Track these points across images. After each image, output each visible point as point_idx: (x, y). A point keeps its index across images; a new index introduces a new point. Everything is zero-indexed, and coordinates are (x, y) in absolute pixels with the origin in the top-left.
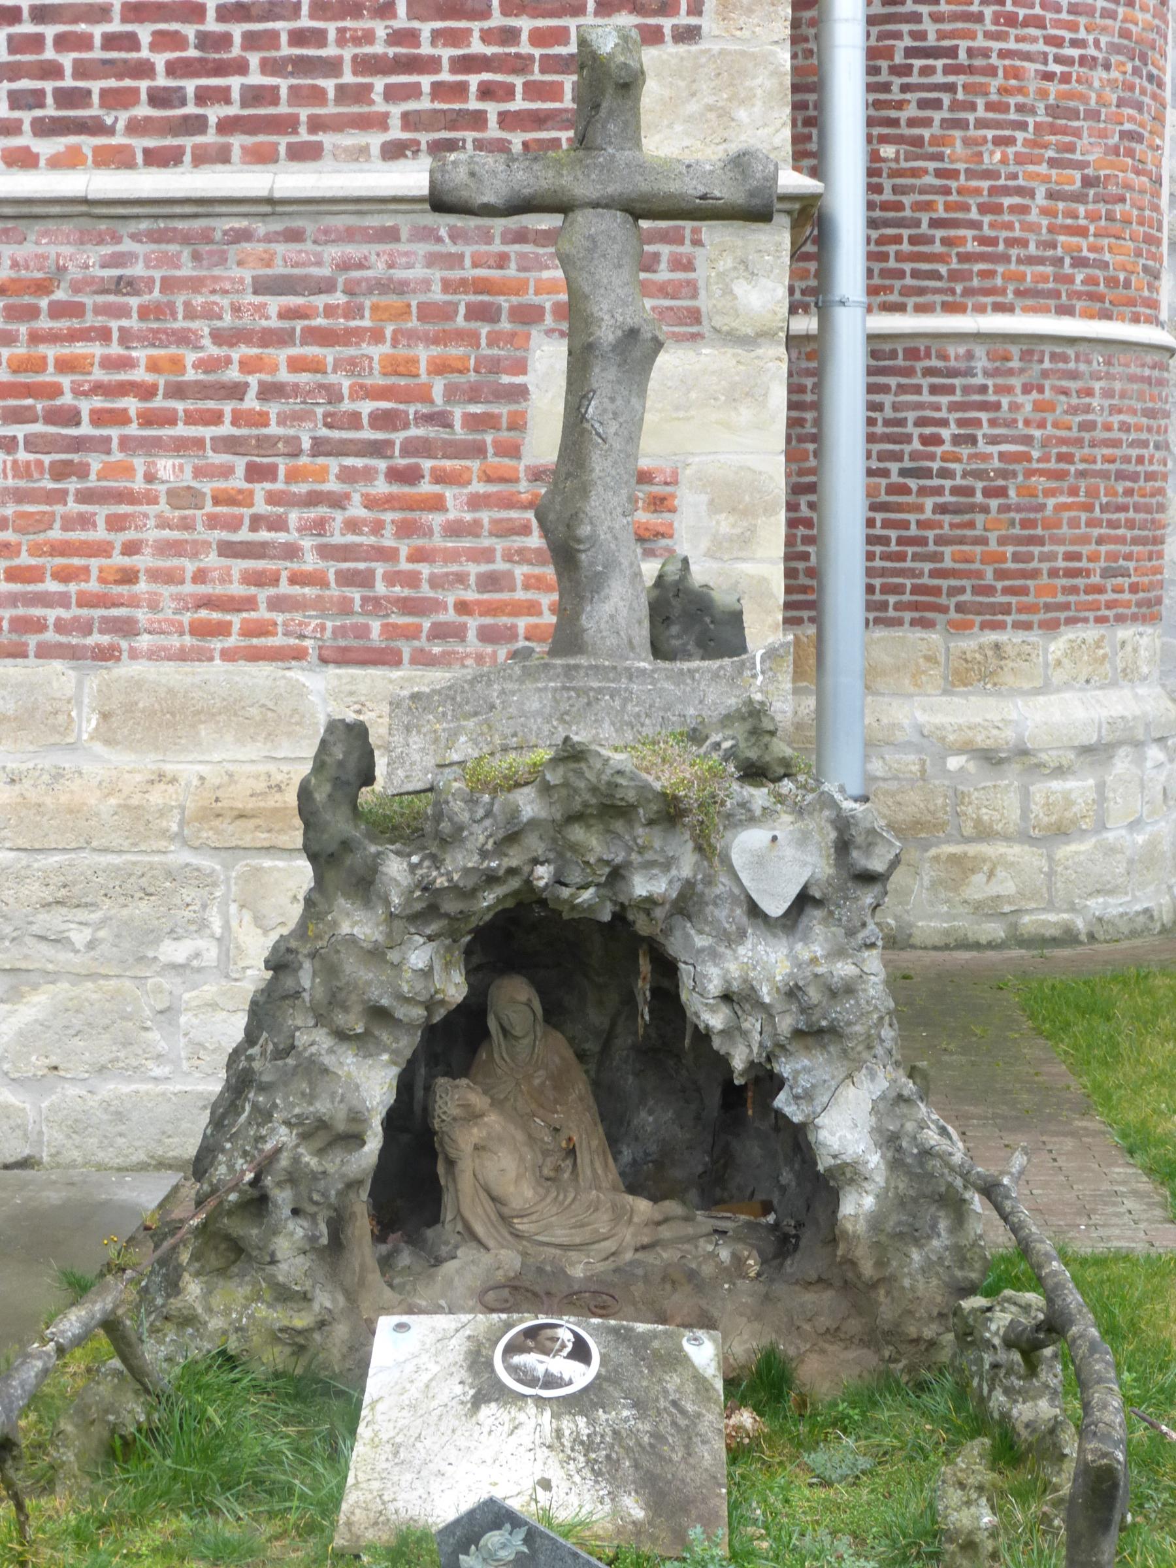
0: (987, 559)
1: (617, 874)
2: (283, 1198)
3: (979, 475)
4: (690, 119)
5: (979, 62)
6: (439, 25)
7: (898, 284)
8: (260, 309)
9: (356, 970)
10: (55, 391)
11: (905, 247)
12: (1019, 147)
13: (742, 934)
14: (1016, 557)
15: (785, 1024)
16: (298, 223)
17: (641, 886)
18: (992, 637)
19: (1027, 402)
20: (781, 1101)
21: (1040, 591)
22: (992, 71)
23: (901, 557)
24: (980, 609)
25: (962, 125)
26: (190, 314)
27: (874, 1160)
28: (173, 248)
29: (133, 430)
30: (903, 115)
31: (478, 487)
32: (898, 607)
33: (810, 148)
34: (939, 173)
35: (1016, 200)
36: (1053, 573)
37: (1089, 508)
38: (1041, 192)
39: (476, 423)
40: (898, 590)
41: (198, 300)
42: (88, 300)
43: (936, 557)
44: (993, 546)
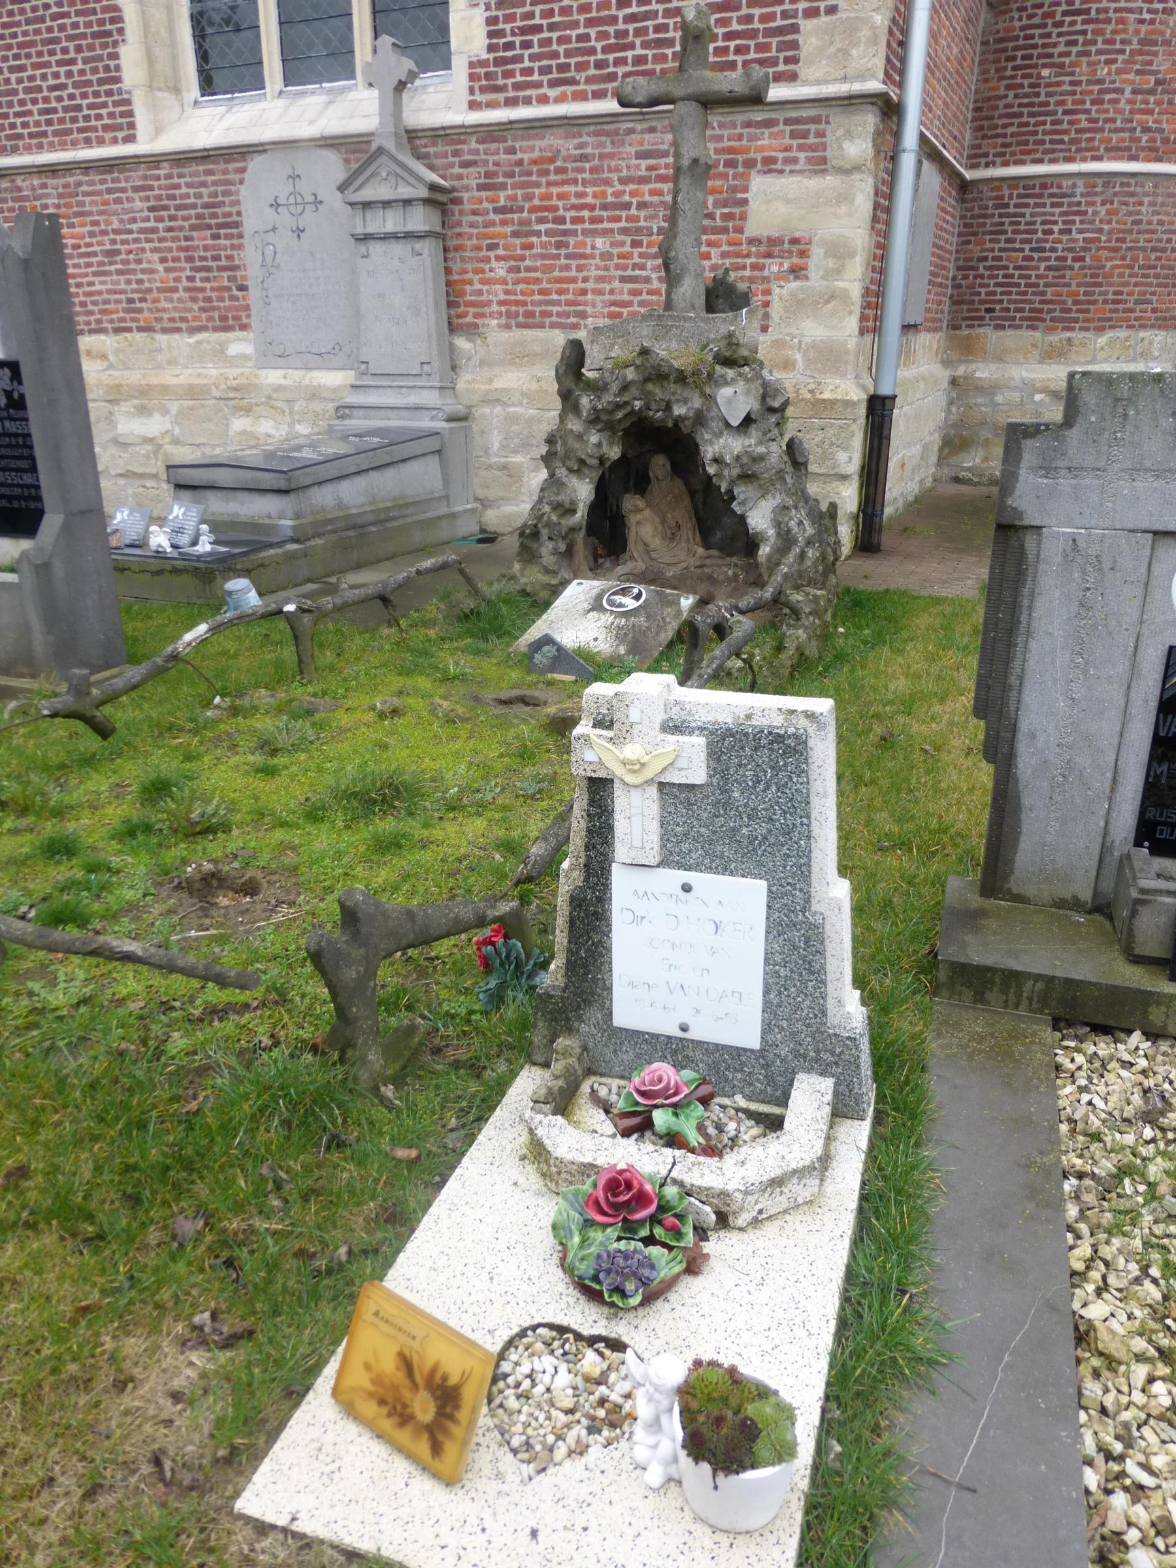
0: (1069, 294)
1: (668, 407)
2: (545, 532)
3: (1071, 250)
4: (829, 57)
5: (1102, 16)
6: (718, 16)
7: (1041, 148)
8: (638, 167)
9: (573, 443)
10: (556, 208)
11: (1048, 127)
12: (1119, 65)
13: (721, 433)
14: (1085, 293)
15: (736, 472)
16: (653, 124)
17: (678, 410)
18: (1068, 334)
19: (1103, 210)
20: (734, 505)
21: (1096, 311)
22: (1109, 21)
23: (1025, 293)
24: (1063, 320)
25: (1087, 54)
26: (610, 171)
27: (771, 532)
28: (603, 139)
29: (587, 226)
30: (1056, 51)
31: (725, 248)
32: (1021, 319)
33: (896, 69)
34: (1072, 83)
35: (1114, 96)
36: (1105, 302)
37: (1131, 267)
38: (1128, 90)
39: (727, 217)
40: (1022, 310)
41: (613, 163)
42: (569, 165)
43: (1044, 293)
44: (1074, 287)
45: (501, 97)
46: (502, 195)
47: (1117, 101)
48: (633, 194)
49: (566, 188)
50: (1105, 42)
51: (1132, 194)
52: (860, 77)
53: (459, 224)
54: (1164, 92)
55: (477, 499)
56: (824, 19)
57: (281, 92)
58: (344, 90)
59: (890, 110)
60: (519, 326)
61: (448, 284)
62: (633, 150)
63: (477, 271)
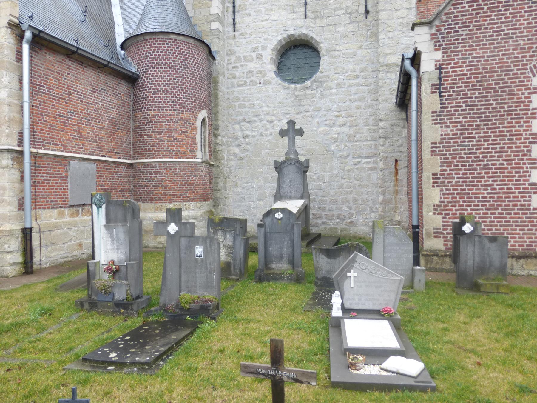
3: (158, 181)
18: (161, 204)
19: (165, 171)
25: (154, 132)
33: (21, 142)
36: (170, 195)
38: (166, 141)
43: (152, 193)
47: (163, 144)
52: (4, 145)
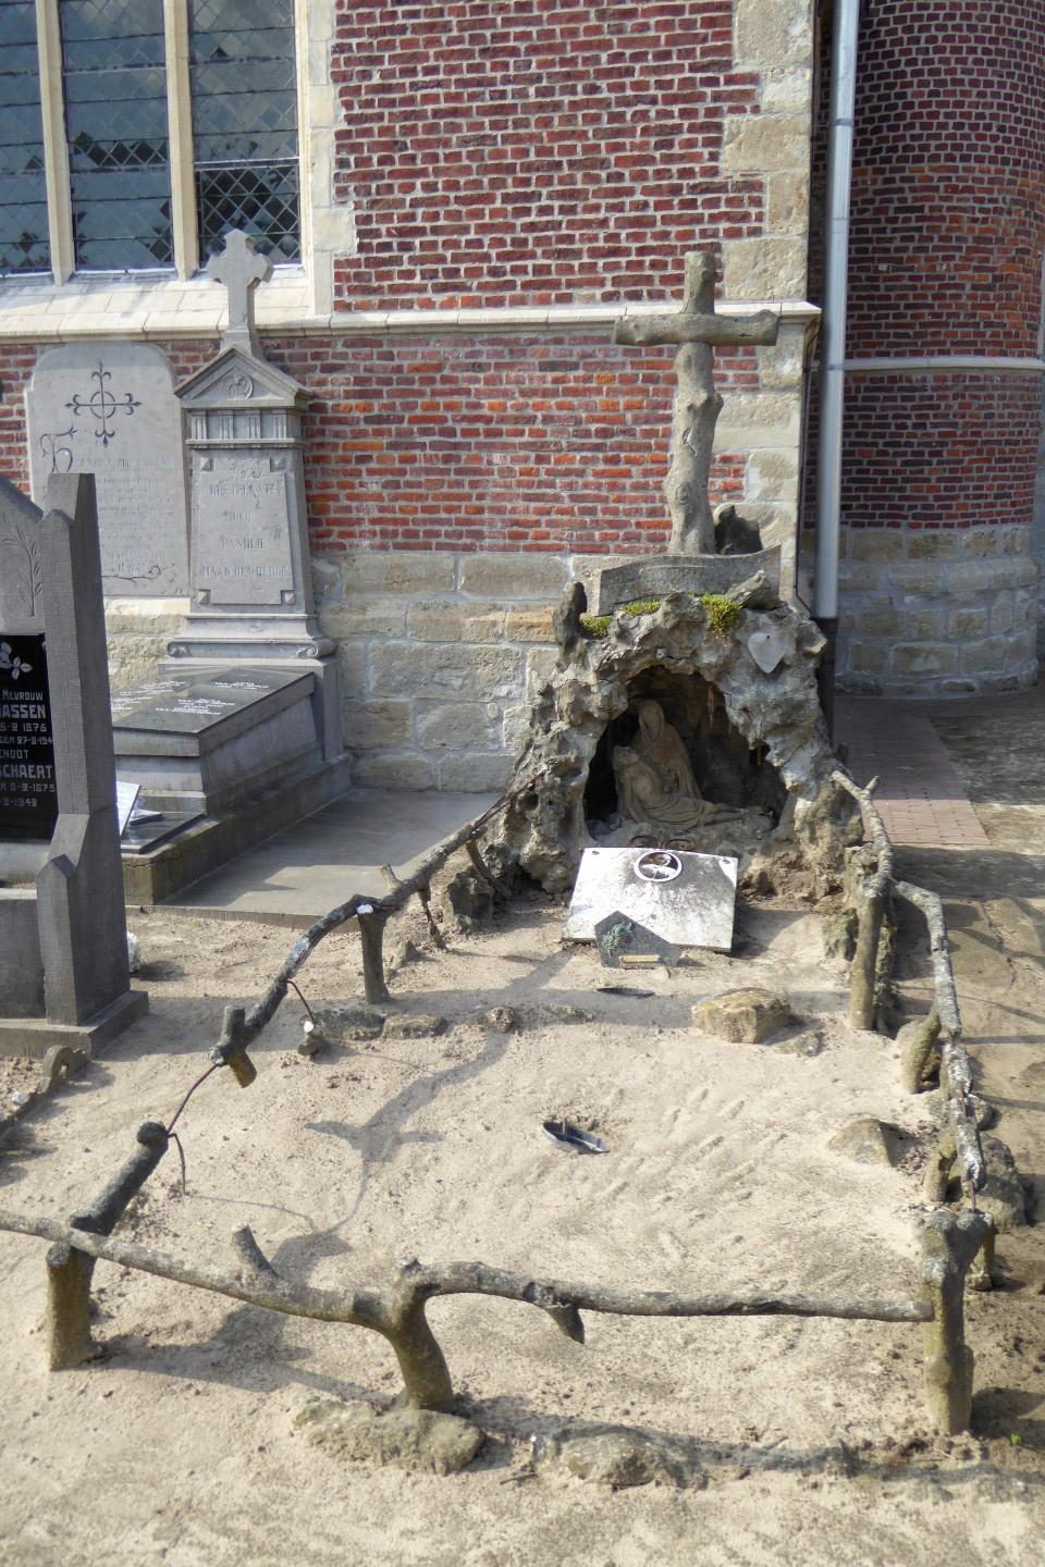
3: (928, 444)
5: (936, 214)
8: (543, 380)
10: (444, 420)
11: (891, 320)
14: (946, 489)
19: (955, 404)
24: (925, 517)
25: (925, 250)
28: (500, 348)
29: (482, 439)
30: (892, 246)
34: (911, 278)
35: (954, 291)
36: (967, 497)
38: (968, 286)
40: (881, 507)
41: (513, 374)
45: (375, 299)
46: (376, 403)
47: (958, 296)
48: (537, 407)
49: (456, 399)
50: (941, 239)
51: (983, 388)
53: (322, 432)
54: (1001, 288)
55: (347, 748)
56: (747, 241)
57: (72, 277)
58: (158, 278)
59: (817, 329)
60: (398, 547)
61: (309, 499)
62: (536, 361)
63: (343, 486)
